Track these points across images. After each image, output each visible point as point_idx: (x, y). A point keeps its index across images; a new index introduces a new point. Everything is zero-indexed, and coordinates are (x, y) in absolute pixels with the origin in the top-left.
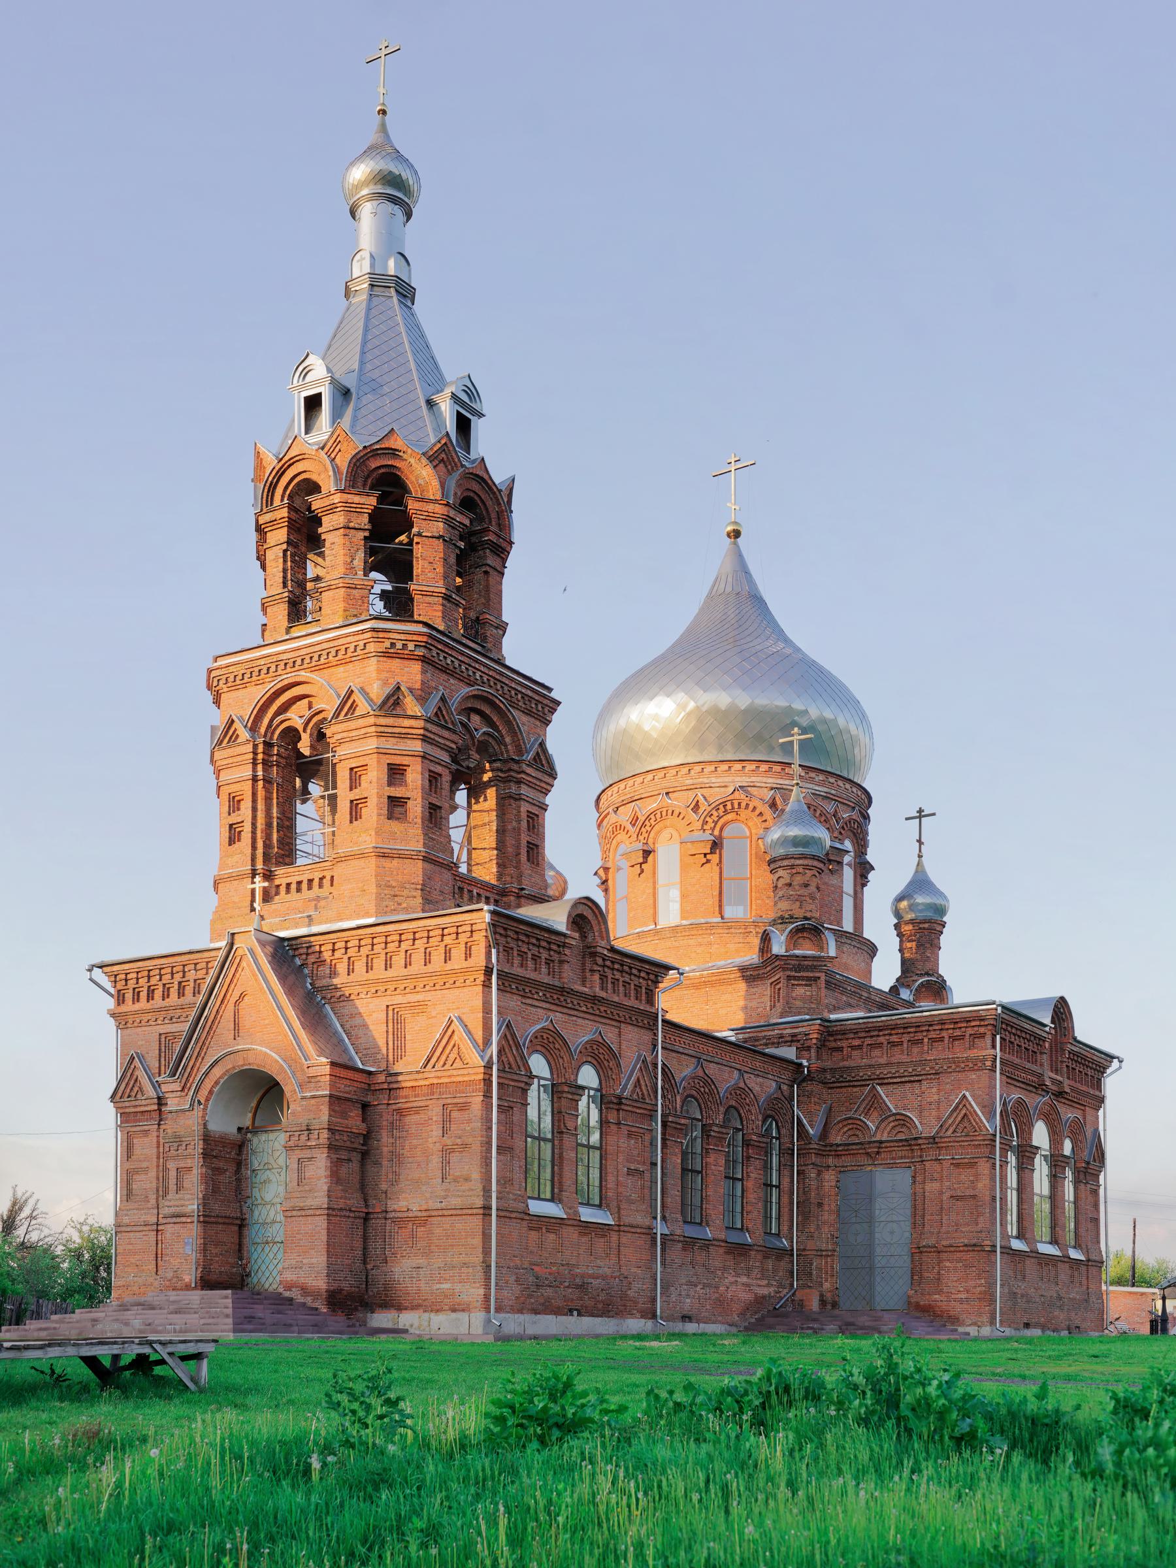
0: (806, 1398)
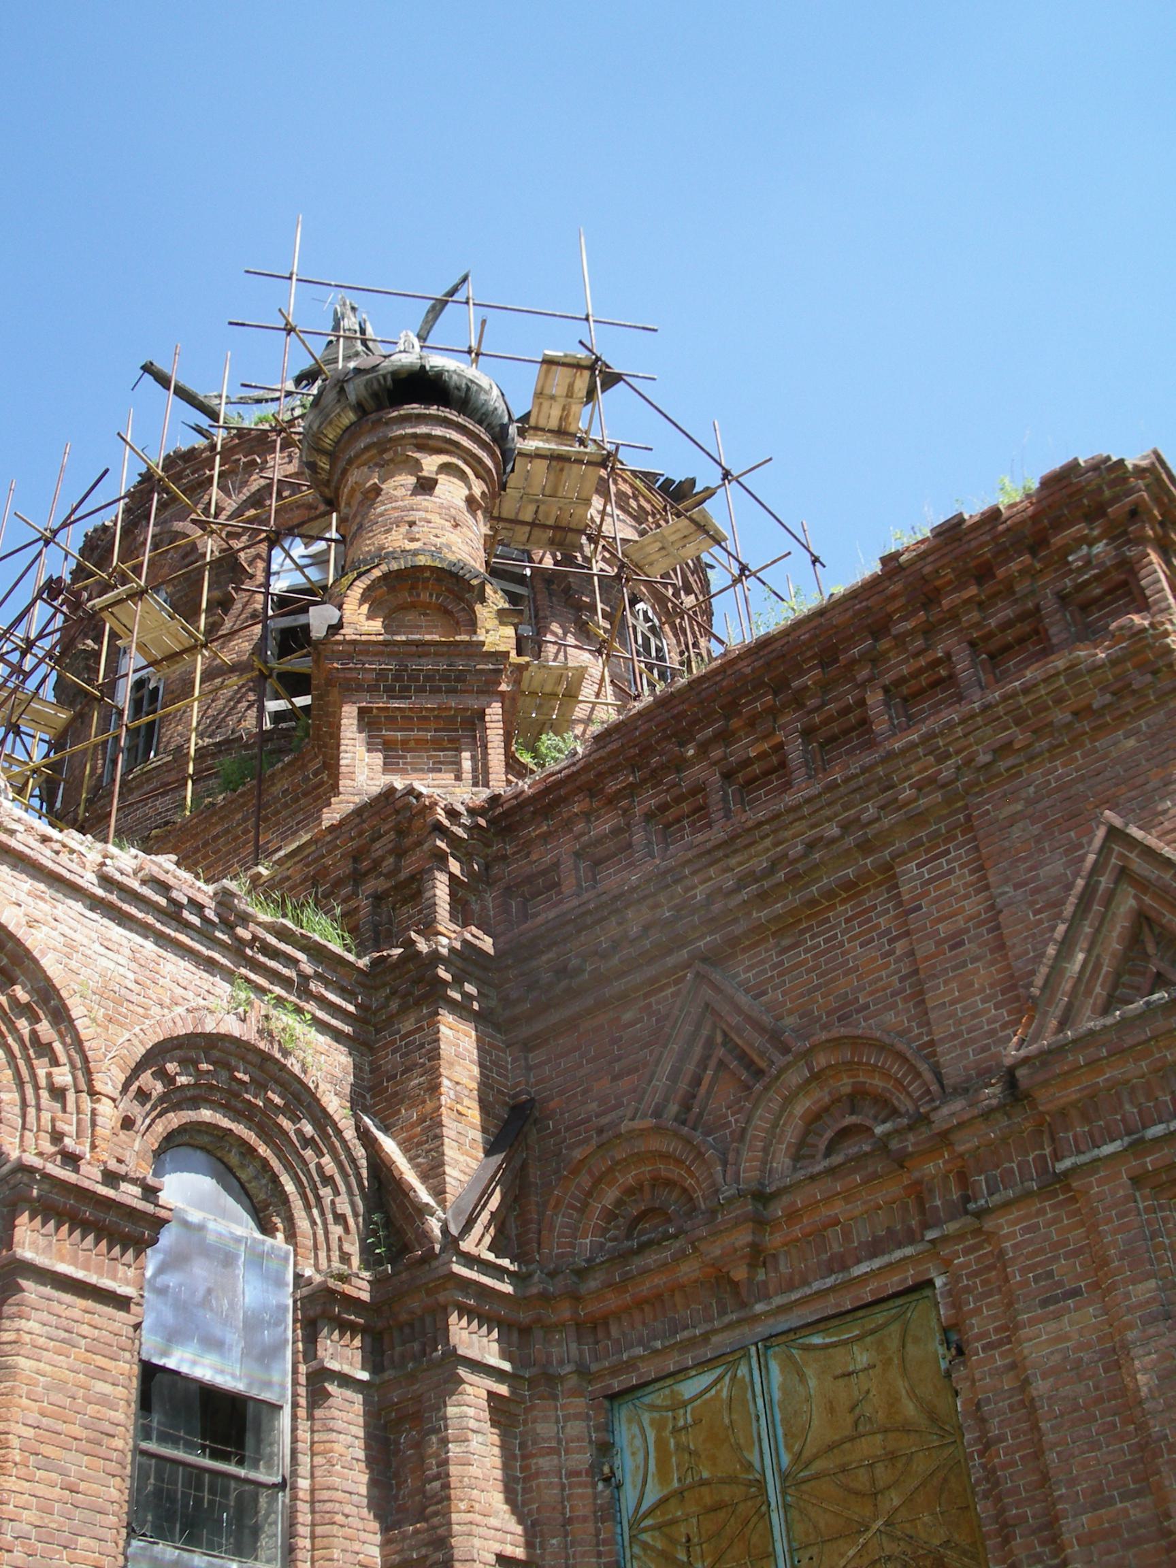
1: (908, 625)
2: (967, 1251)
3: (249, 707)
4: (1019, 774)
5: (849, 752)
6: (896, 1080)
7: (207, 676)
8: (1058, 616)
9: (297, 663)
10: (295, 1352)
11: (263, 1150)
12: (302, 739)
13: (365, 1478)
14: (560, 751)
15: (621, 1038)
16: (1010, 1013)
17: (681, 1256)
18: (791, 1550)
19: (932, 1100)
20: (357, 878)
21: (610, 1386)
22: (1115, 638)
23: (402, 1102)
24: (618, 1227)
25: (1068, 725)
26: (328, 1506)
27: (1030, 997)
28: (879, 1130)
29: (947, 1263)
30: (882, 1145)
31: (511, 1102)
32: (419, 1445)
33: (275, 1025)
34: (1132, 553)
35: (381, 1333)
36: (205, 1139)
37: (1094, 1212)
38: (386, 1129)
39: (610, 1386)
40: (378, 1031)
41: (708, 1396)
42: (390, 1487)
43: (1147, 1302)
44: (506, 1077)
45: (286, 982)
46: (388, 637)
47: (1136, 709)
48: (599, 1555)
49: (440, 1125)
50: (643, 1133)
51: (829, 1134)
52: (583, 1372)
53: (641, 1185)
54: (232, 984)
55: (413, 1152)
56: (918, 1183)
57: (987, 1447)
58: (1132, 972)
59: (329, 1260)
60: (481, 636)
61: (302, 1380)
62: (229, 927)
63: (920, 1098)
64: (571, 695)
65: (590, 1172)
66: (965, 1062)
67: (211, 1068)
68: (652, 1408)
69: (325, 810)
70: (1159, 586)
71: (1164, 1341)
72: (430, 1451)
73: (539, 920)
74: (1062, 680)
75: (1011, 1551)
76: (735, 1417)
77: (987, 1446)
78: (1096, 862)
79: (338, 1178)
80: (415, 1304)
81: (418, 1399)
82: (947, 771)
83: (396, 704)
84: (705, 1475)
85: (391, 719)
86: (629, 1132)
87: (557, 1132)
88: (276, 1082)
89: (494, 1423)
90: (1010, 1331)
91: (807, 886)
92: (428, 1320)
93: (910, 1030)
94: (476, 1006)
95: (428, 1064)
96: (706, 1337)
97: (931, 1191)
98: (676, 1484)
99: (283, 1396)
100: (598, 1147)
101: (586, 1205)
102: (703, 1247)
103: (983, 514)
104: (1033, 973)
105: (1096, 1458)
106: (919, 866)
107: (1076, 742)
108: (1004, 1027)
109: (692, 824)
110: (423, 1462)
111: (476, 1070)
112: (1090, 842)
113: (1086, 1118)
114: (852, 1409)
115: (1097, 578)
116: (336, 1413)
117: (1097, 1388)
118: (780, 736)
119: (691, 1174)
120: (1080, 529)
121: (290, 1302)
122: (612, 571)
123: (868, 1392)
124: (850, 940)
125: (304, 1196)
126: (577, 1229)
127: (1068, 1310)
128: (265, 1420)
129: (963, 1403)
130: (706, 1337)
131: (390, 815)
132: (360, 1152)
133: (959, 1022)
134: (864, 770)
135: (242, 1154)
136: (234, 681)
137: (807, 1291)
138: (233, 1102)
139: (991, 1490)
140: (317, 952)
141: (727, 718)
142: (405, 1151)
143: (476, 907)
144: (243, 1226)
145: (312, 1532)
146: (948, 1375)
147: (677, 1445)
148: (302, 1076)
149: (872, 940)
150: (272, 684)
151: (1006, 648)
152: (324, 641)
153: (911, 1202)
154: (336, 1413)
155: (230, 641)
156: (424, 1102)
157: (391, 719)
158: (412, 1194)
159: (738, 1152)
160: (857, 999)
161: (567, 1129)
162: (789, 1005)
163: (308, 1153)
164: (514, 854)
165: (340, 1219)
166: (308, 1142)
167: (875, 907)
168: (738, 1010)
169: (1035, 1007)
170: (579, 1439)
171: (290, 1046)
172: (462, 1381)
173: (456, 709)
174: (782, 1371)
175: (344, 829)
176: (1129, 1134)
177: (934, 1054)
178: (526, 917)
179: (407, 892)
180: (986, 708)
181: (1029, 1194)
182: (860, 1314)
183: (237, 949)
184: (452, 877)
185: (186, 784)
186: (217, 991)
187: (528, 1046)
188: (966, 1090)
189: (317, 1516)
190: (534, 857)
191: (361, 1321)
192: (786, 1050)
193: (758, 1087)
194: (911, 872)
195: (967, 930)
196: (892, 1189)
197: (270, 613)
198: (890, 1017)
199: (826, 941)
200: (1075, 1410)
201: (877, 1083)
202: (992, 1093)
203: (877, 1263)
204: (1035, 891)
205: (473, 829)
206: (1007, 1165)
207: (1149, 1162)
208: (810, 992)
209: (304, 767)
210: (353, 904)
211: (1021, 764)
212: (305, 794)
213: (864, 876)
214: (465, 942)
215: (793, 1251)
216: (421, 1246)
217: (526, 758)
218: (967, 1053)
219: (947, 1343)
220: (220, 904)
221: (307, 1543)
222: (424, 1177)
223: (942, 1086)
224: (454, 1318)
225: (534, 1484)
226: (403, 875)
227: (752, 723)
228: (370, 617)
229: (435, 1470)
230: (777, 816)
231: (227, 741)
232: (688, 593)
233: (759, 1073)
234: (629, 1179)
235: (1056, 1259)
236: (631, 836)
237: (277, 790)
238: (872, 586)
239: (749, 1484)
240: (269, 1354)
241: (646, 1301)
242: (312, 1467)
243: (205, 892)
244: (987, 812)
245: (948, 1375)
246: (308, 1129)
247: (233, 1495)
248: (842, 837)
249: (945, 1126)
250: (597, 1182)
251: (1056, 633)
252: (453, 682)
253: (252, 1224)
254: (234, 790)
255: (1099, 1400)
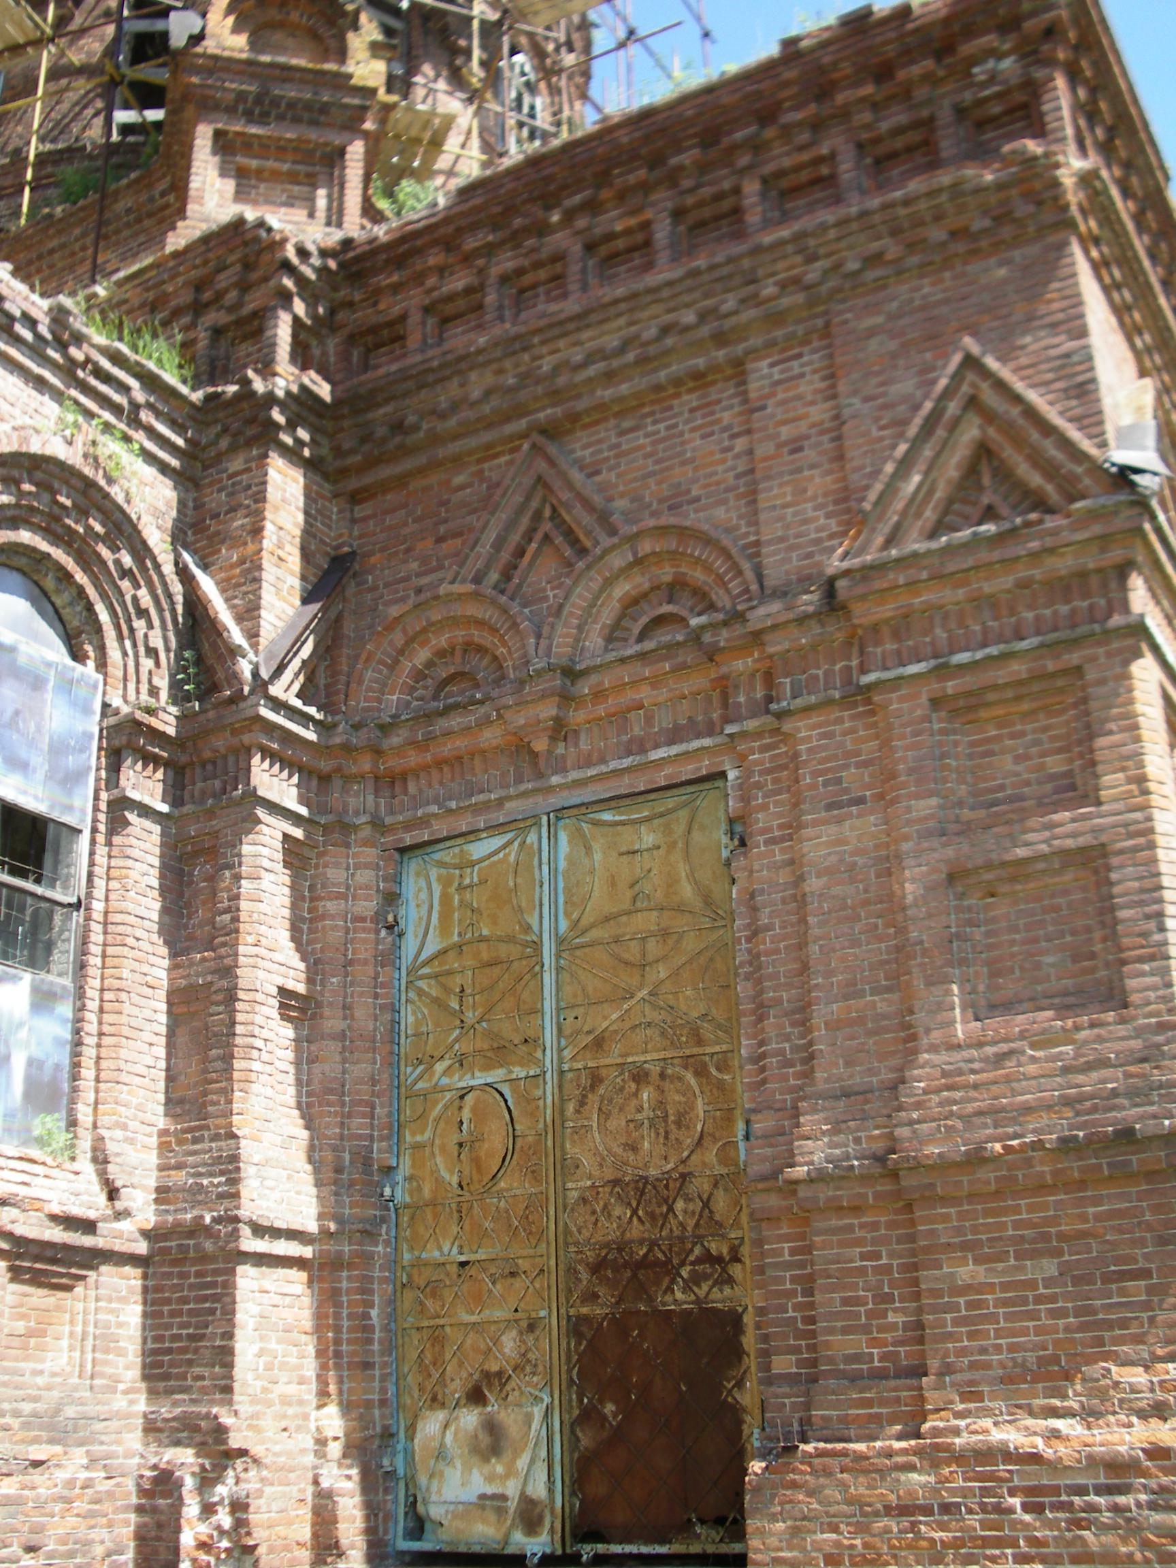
0: (1116, 998)
1: (798, 116)
2: (764, 749)
3: (96, 114)
4: (884, 287)
5: (719, 240)
6: (717, 575)
7: (53, 75)
8: (951, 130)
9: (150, 72)
10: (98, 780)
11: (80, 577)
12: (150, 157)
13: (157, 905)
14: (419, 200)
15: (448, 501)
16: (839, 524)
17: (486, 722)
18: (559, 1009)
19: (750, 599)
20: (198, 308)
21: (401, 840)
22: (1006, 161)
23: (223, 542)
24: (426, 688)
25: (943, 244)
26: (120, 929)
27: (861, 511)
28: (694, 622)
29: (743, 757)
30: (696, 637)
31: (333, 553)
32: (212, 879)
33: (102, 452)
34: (1039, 74)
35: (183, 768)
36: (22, 562)
37: (890, 727)
38: (205, 567)
39: (401, 840)
40: (205, 468)
41: (496, 858)
42: (182, 916)
43: (926, 818)
44: (330, 528)
45: (116, 409)
46: (252, 56)
47: (1015, 238)
48: (376, 996)
49: (260, 568)
50: (460, 597)
51: (644, 620)
52: (377, 824)
53: (453, 649)
54: (61, 405)
55: (230, 593)
56: (725, 677)
57: (755, 933)
58: (964, 501)
59: (138, 692)
60: (350, 68)
61: (103, 806)
62: (62, 346)
63: (738, 596)
64: (436, 144)
65: (404, 631)
66: (787, 567)
67: (33, 489)
68: (441, 864)
69: (170, 234)
70: (1057, 114)
71: (936, 855)
72: (223, 885)
73: (382, 371)
74: (944, 197)
75: (763, 1029)
76: (519, 880)
77: (755, 933)
78: (947, 388)
79: (153, 612)
80: (220, 742)
81: (215, 834)
82: (813, 274)
83: (254, 130)
84: (485, 932)
85: (247, 145)
86: (447, 595)
87: (374, 588)
88: (99, 509)
89: (287, 864)
90: (793, 829)
91: (655, 370)
92: (231, 759)
93: (737, 528)
94: (307, 452)
95: (253, 506)
96: (500, 802)
97: (737, 687)
98: (456, 938)
99: (83, 821)
100: (416, 607)
101: (396, 662)
102: (508, 715)
103: (894, 8)
104: (867, 488)
105: (855, 954)
106: (772, 365)
107: (947, 263)
108: (832, 536)
109: (548, 293)
110: (215, 895)
111: (301, 518)
112: (945, 366)
113: (896, 635)
114: (632, 886)
115: (998, 96)
116: (134, 841)
117: (866, 891)
118: (649, 214)
119: (504, 644)
120: (989, 40)
121: (96, 730)
122: (494, 16)
123: (649, 871)
124: (693, 430)
125: (118, 627)
126: (385, 685)
127: (850, 816)
128: (63, 843)
129: (739, 892)
130: (500, 802)
131: (237, 247)
132: (177, 588)
133: (787, 527)
134: (730, 260)
135: (59, 580)
136: (82, 85)
137: (604, 768)
138: (54, 526)
139: (751, 973)
140: (150, 381)
141: (598, 187)
142: (223, 591)
143: (316, 352)
144: (54, 650)
145: (104, 952)
146: (728, 863)
147: (461, 901)
148: (125, 506)
149: (712, 434)
150: (122, 92)
151: (893, 156)
152: (184, 51)
153: (716, 695)
154: (134, 841)
155: (79, 38)
156: (245, 544)
157: (247, 145)
158: (225, 634)
159: (552, 626)
160: (688, 491)
161: (386, 585)
162: (621, 488)
163: (125, 584)
164: (362, 301)
165: (152, 652)
166: (125, 573)
167: (719, 401)
168: (570, 486)
169: (863, 523)
170: (367, 887)
171: (115, 474)
172: (259, 822)
173: (317, 144)
174: (570, 842)
175: (189, 256)
176: (935, 657)
177: (758, 554)
178: (366, 367)
179: (247, 328)
180: (864, 214)
181: (829, 702)
182: (653, 796)
183: (69, 370)
184: (296, 319)
185: (22, 191)
186: (45, 410)
187: (355, 498)
188: (785, 594)
189: (109, 937)
190: (382, 306)
191: (165, 755)
192: (613, 532)
193: (581, 565)
194: (763, 372)
195: (807, 437)
196: (698, 681)
197: (126, 13)
198: (720, 513)
199: (668, 428)
200: (843, 909)
201: (698, 576)
202: (809, 600)
203: (674, 750)
204: (884, 407)
205: (322, 271)
206: (813, 671)
207: (951, 686)
208: (644, 477)
209: (150, 186)
210: (192, 335)
211: (887, 277)
212: (150, 215)
213: (715, 368)
214: (303, 388)
215: (596, 729)
216: (230, 686)
217: (383, 204)
218: (790, 559)
219: (731, 834)
220: (55, 320)
221: (98, 961)
222: (239, 619)
223: (762, 587)
224: (256, 760)
225: (320, 925)
226: (246, 310)
227: (621, 196)
228: (236, 30)
229: (226, 903)
230: (634, 296)
231: (69, 150)
232: (571, 50)
233: (582, 551)
234: (442, 641)
235: (846, 767)
236: (484, 296)
237: (120, 206)
238: (767, 69)
239: (525, 945)
240: (71, 780)
241: (446, 761)
242: (108, 890)
243: (39, 306)
244: (846, 322)
245: (728, 863)
246: (127, 560)
247: (29, 911)
248: (696, 326)
249: (759, 626)
250: (410, 641)
251: (947, 147)
252: (316, 114)
253: (63, 649)
254: (75, 203)
255: (866, 903)
